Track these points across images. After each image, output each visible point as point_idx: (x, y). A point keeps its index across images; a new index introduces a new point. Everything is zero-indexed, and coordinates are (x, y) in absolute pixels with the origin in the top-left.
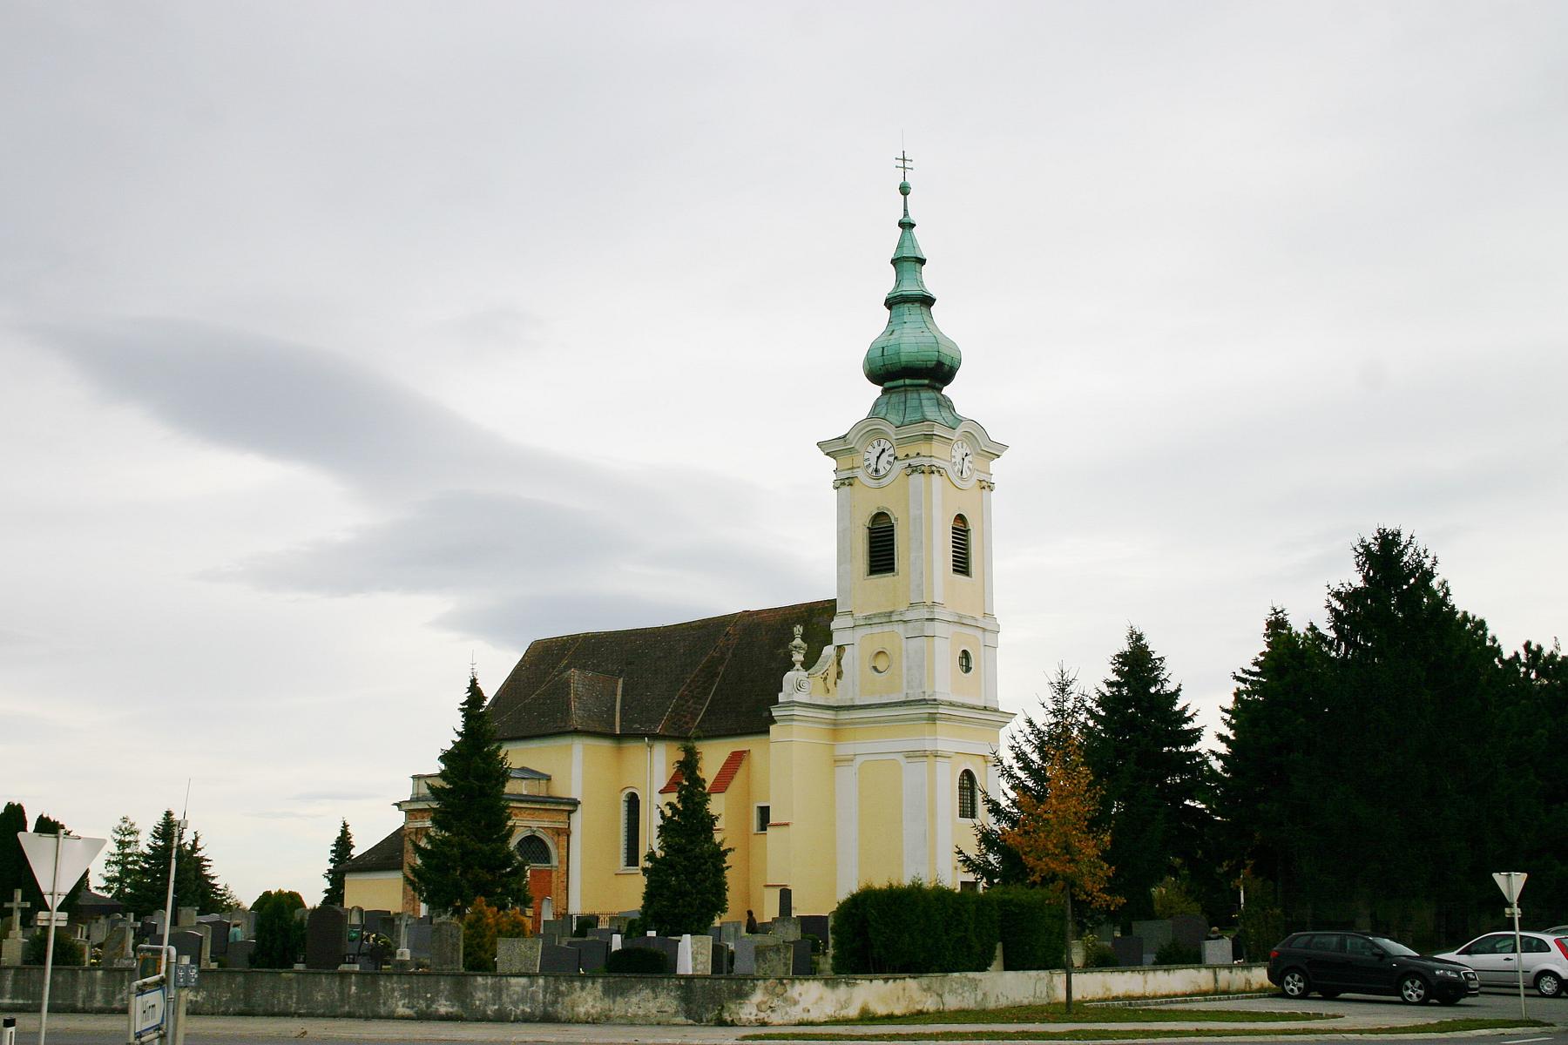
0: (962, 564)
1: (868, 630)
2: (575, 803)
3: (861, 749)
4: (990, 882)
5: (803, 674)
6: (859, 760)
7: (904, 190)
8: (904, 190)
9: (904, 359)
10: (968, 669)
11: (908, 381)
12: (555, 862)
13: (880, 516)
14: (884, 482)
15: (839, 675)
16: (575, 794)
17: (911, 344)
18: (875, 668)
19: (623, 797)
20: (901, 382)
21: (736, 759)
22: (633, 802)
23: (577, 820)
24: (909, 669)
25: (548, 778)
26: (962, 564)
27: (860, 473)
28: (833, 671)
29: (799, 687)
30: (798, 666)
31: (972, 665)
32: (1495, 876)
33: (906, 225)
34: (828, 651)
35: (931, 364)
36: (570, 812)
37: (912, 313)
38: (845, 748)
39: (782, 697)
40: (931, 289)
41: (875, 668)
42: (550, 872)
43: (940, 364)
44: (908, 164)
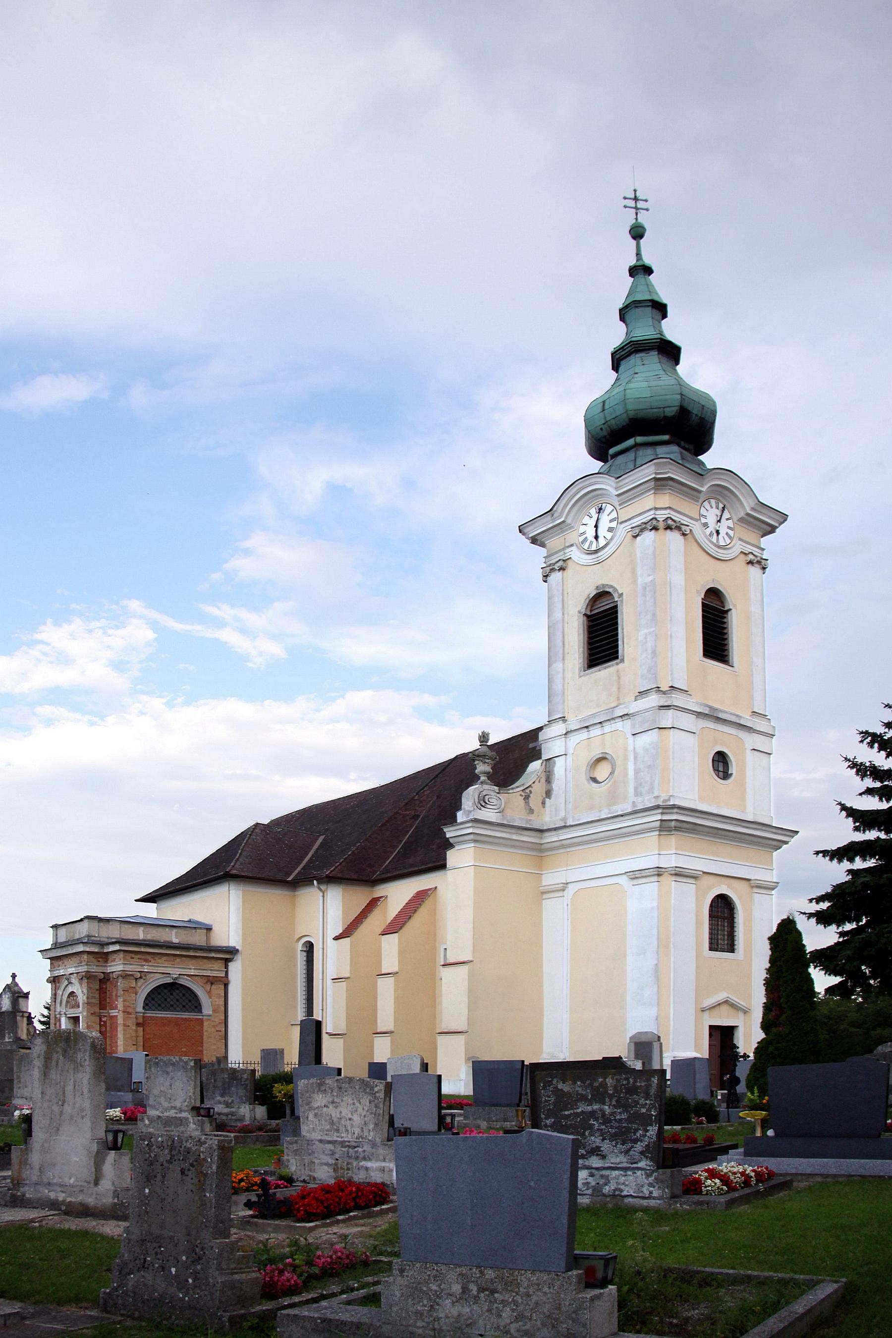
0: (716, 643)
1: (584, 735)
2: (232, 952)
3: (573, 875)
4: (584, 1132)
5: (490, 789)
6: (572, 889)
7: (637, 233)
8: (637, 233)
9: (631, 407)
10: (726, 775)
11: (639, 439)
12: (207, 1010)
13: (602, 595)
14: (603, 554)
15: (548, 794)
16: (233, 941)
17: (647, 382)
18: (594, 780)
19: (300, 946)
20: (631, 442)
21: (421, 897)
22: (309, 948)
23: (236, 970)
24: (637, 772)
25: (209, 929)
26: (716, 643)
27: (575, 554)
28: (539, 789)
29: (483, 802)
30: (483, 778)
31: (733, 769)
32: (811, 970)
33: (641, 270)
34: (535, 766)
35: (671, 412)
36: (227, 961)
37: (641, 278)
38: (551, 878)
39: (460, 816)
40: (664, 297)
41: (594, 780)
42: (200, 1022)
43: (683, 412)
44: (640, 205)
